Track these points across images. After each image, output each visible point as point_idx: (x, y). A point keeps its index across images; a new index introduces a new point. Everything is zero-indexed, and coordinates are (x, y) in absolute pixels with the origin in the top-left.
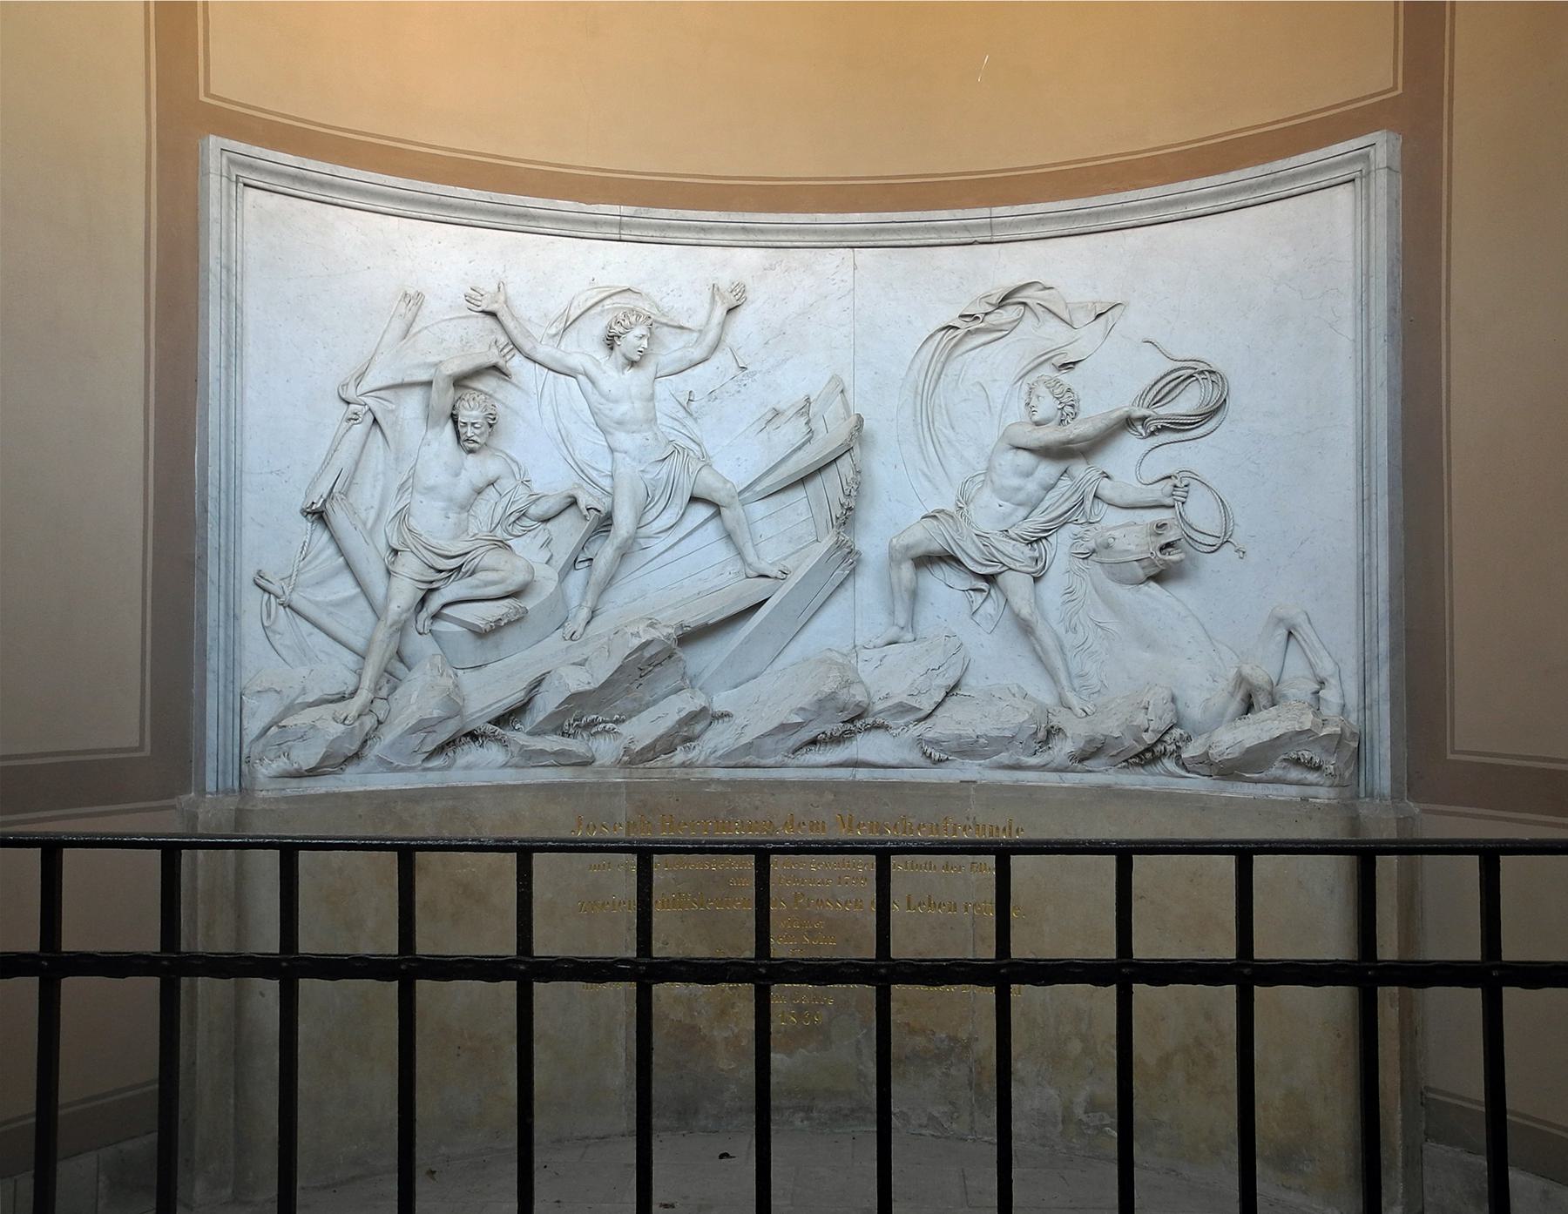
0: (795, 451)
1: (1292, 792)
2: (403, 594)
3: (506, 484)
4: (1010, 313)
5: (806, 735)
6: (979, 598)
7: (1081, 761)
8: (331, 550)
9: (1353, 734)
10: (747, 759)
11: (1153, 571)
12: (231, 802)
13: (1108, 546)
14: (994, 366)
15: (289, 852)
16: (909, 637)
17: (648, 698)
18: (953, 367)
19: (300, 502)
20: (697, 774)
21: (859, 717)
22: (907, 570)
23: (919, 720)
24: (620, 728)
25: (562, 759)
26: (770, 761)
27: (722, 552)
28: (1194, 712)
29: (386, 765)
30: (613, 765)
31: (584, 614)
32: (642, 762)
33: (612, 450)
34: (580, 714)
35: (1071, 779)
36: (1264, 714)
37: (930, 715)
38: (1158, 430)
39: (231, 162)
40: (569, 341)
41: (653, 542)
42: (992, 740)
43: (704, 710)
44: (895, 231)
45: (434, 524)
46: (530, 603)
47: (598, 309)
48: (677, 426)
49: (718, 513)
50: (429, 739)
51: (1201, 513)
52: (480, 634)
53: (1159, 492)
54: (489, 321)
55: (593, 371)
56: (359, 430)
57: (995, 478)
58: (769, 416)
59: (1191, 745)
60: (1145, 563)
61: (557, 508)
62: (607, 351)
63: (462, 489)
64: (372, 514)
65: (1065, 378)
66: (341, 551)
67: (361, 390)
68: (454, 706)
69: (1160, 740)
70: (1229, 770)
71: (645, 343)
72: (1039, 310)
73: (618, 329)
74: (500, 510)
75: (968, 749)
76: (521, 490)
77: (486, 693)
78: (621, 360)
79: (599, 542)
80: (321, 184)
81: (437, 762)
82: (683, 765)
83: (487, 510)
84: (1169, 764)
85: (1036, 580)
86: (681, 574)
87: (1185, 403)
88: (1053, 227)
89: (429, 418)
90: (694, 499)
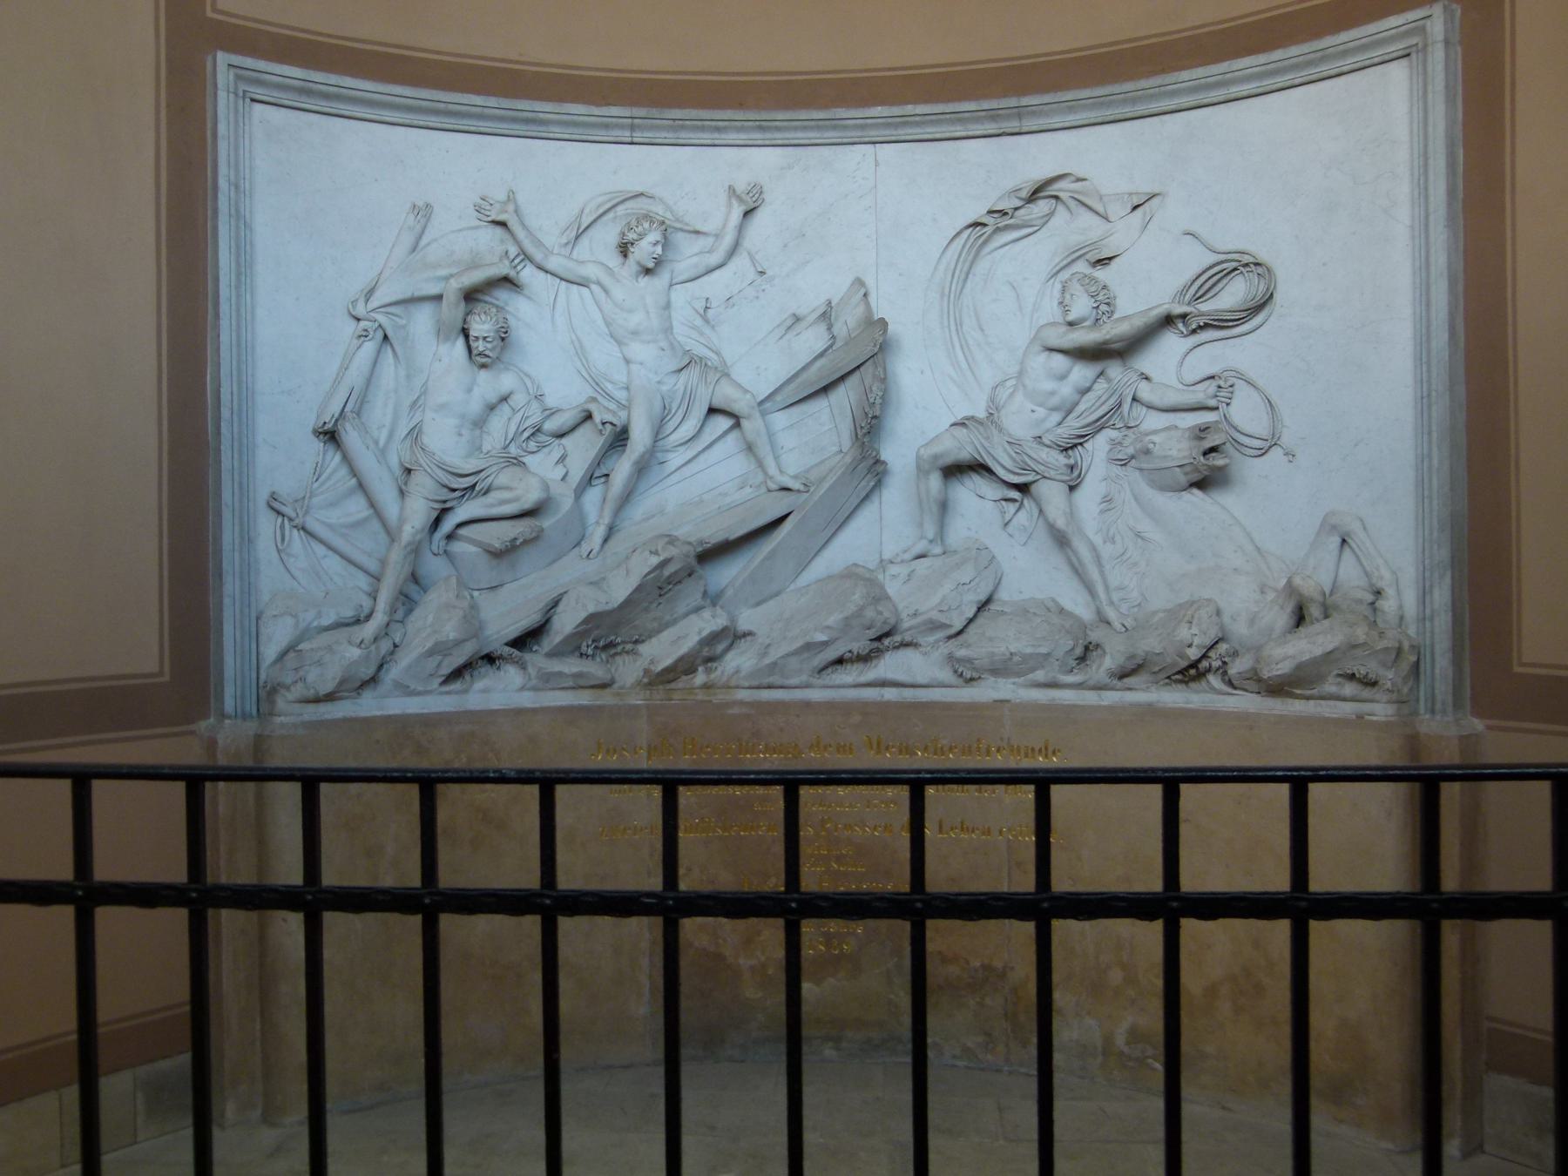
0: (816, 359)
1: (1347, 709)
2: (418, 512)
3: (519, 399)
4: (1042, 206)
5: (832, 654)
6: (1012, 508)
7: (1122, 676)
8: (344, 471)
9: (1412, 647)
10: (771, 680)
11: (1196, 477)
12: (251, 727)
13: (1147, 452)
14: (1025, 270)
15: (310, 782)
16: (938, 550)
17: (667, 618)
18: (982, 266)
19: (311, 421)
20: (720, 697)
21: (887, 634)
22: (935, 481)
23: (950, 637)
24: (642, 648)
25: (580, 683)
26: (794, 681)
27: (740, 465)
28: (1240, 629)
29: (406, 691)
30: (633, 687)
32: (663, 683)
33: (627, 361)
34: (606, 634)
35: (1110, 698)
36: (1317, 627)
38: (1200, 327)
39: (238, 78)
40: (583, 249)
42: (1026, 658)
43: (725, 630)
44: (918, 124)
45: (446, 443)
47: (611, 215)
48: (695, 335)
49: (737, 425)
50: (446, 662)
51: (1245, 413)
52: (497, 555)
53: (1200, 394)
54: (499, 231)
55: (606, 280)
56: (369, 347)
57: (1027, 382)
58: (789, 322)
59: (1238, 661)
60: (1188, 469)
61: (571, 423)
62: (620, 259)
63: (475, 406)
65: (1101, 274)
66: (354, 472)
67: (371, 305)
68: (472, 620)
69: (1204, 656)
70: (1278, 688)
71: (659, 250)
72: (1072, 204)
73: (631, 236)
75: (1001, 669)
76: (535, 405)
77: (504, 616)
78: (635, 268)
80: (327, 96)
81: (456, 686)
82: (707, 686)
83: (500, 427)
84: (1214, 680)
86: (703, 485)
87: (1229, 299)
88: (1084, 115)
89: (441, 333)
90: (712, 411)
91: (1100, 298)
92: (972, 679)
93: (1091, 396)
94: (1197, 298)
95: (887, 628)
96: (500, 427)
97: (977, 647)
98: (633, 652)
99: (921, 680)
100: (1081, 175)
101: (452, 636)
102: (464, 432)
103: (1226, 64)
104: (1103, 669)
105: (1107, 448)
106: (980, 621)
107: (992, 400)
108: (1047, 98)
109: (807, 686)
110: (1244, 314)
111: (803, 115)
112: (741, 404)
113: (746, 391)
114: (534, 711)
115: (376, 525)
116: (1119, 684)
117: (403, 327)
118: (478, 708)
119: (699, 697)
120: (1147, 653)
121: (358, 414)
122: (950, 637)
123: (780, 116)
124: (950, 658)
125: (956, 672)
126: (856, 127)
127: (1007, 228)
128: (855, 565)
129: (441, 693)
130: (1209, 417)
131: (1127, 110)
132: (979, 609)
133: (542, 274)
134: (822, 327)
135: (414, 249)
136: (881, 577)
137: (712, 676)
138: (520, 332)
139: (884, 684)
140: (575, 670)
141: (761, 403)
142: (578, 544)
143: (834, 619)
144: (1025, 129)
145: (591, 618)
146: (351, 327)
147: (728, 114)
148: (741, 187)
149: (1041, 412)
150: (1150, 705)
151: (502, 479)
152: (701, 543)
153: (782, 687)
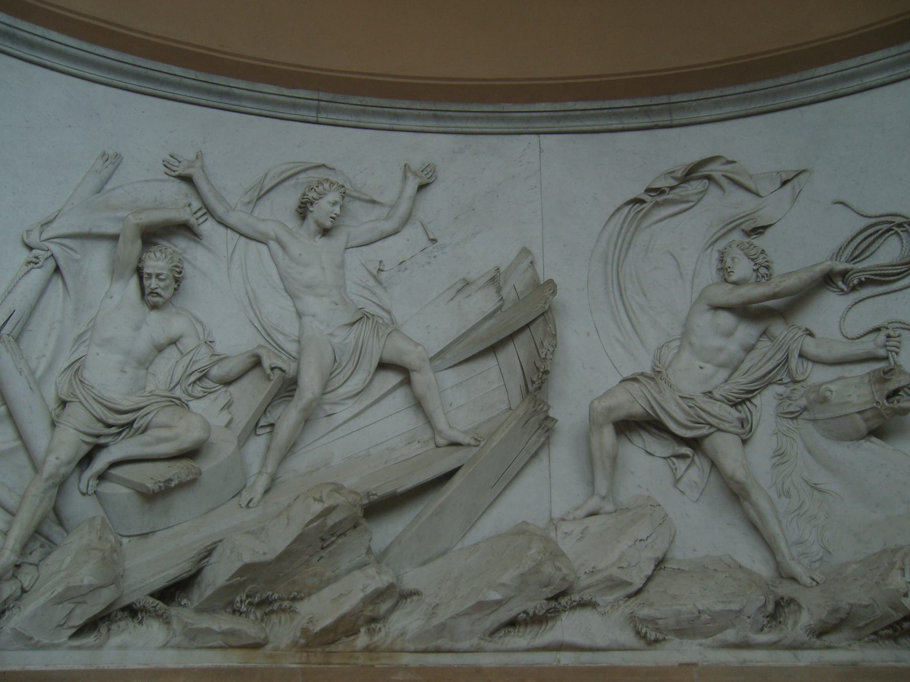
2: (69, 443)
3: (188, 343)
4: (695, 187)
5: (504, 615)
6: (681, 465)
10: (439, 643)
11: (875, 423)
13: (824, 400)
14: (683, 241)
17: (329, 574)
20: (384, 661)
21: (563, 594)
22: (608, 434)
23: (630, 596)
26: (465, 645)
27: (408, 421)
31: (263, 481)
33: (300, 315)
34: (262, 589)
35: (807, 658)
37: (639, 592)
40: (264, 208)
41: (338, 409)
43: (391, 587)
44: (578, 118)
46: (206, 465)
47: (292, 181)
48: (367, 294)
49: (407, 381)
50: (78, 611)
52: (150, 497)
53: (868, 345)
54: (184, 187)
55: (285, 237)
56: (38, 276)
58: (459, 286)
60: (869, 415)
63: (142, 345)
64: (44, 364)
68: (112, 566)
71: (337, 209)
72: (725, 182)
73: (312, 195)
74: (180, 371)
76: (204, 350)
77: (149, 565)
79: (282, 407)
80: (31, 45)
81: (90, 640)
83: (167, 368)
85: (744, 442)
86: (368, 439)
89: (115, 272)
91: (760, 261)
92: (656, 641)
93: (755, 355)
94: (853, 259)
95: (565, 586)
96: (167, 368)
97: (660, 605)
98: (291, 611)
99: (601, 642)
100: (730, 159)
101: (86, 581)
102: (127, 369)
103: (859, 58)
104: (800, 625)
105: (775, 403)
106: (658, 579)
107: (658, 358)
108: (694, 96)
109: (478, 650)
110: (904, 268)
111: (475, 107)
112: (412, 357)
113: (417, 345)
114: (176, 672)
115: (22, 458)
116: (818, 642)
117: (77, 261)
118: (112, 667)
119: (360, 662)
120: (852, 605)
121: (17, 340)
122: (630, 596)
123: (454, 107)
124: (633, 619)
125: (638, 633)
126: (521, 119)
127: (666, 203)
128: (525, 523)
129: (71, 648)
130: (882, 365)
131: (769, 104)
132: (656, 566)
133: (222, 230)
134: (491, 291)
135: (99, 190)
136: (552, 534)
137: (376, 638)
138: (192, 280)
139: (560, 647)
140: (225, 626)
141: (431, 359)
142: (239, 493)
143: (509, 576)
144: (675, 122)
145: (247, 569)
146: (25, 255)
147: (406, 104)
148: (416, 165)
149: (709, 368)
150: (854, 664)
151: (163, 417)
152: (368, 495)
153: (450, 651)
